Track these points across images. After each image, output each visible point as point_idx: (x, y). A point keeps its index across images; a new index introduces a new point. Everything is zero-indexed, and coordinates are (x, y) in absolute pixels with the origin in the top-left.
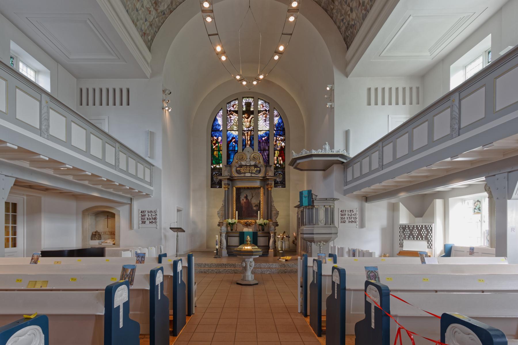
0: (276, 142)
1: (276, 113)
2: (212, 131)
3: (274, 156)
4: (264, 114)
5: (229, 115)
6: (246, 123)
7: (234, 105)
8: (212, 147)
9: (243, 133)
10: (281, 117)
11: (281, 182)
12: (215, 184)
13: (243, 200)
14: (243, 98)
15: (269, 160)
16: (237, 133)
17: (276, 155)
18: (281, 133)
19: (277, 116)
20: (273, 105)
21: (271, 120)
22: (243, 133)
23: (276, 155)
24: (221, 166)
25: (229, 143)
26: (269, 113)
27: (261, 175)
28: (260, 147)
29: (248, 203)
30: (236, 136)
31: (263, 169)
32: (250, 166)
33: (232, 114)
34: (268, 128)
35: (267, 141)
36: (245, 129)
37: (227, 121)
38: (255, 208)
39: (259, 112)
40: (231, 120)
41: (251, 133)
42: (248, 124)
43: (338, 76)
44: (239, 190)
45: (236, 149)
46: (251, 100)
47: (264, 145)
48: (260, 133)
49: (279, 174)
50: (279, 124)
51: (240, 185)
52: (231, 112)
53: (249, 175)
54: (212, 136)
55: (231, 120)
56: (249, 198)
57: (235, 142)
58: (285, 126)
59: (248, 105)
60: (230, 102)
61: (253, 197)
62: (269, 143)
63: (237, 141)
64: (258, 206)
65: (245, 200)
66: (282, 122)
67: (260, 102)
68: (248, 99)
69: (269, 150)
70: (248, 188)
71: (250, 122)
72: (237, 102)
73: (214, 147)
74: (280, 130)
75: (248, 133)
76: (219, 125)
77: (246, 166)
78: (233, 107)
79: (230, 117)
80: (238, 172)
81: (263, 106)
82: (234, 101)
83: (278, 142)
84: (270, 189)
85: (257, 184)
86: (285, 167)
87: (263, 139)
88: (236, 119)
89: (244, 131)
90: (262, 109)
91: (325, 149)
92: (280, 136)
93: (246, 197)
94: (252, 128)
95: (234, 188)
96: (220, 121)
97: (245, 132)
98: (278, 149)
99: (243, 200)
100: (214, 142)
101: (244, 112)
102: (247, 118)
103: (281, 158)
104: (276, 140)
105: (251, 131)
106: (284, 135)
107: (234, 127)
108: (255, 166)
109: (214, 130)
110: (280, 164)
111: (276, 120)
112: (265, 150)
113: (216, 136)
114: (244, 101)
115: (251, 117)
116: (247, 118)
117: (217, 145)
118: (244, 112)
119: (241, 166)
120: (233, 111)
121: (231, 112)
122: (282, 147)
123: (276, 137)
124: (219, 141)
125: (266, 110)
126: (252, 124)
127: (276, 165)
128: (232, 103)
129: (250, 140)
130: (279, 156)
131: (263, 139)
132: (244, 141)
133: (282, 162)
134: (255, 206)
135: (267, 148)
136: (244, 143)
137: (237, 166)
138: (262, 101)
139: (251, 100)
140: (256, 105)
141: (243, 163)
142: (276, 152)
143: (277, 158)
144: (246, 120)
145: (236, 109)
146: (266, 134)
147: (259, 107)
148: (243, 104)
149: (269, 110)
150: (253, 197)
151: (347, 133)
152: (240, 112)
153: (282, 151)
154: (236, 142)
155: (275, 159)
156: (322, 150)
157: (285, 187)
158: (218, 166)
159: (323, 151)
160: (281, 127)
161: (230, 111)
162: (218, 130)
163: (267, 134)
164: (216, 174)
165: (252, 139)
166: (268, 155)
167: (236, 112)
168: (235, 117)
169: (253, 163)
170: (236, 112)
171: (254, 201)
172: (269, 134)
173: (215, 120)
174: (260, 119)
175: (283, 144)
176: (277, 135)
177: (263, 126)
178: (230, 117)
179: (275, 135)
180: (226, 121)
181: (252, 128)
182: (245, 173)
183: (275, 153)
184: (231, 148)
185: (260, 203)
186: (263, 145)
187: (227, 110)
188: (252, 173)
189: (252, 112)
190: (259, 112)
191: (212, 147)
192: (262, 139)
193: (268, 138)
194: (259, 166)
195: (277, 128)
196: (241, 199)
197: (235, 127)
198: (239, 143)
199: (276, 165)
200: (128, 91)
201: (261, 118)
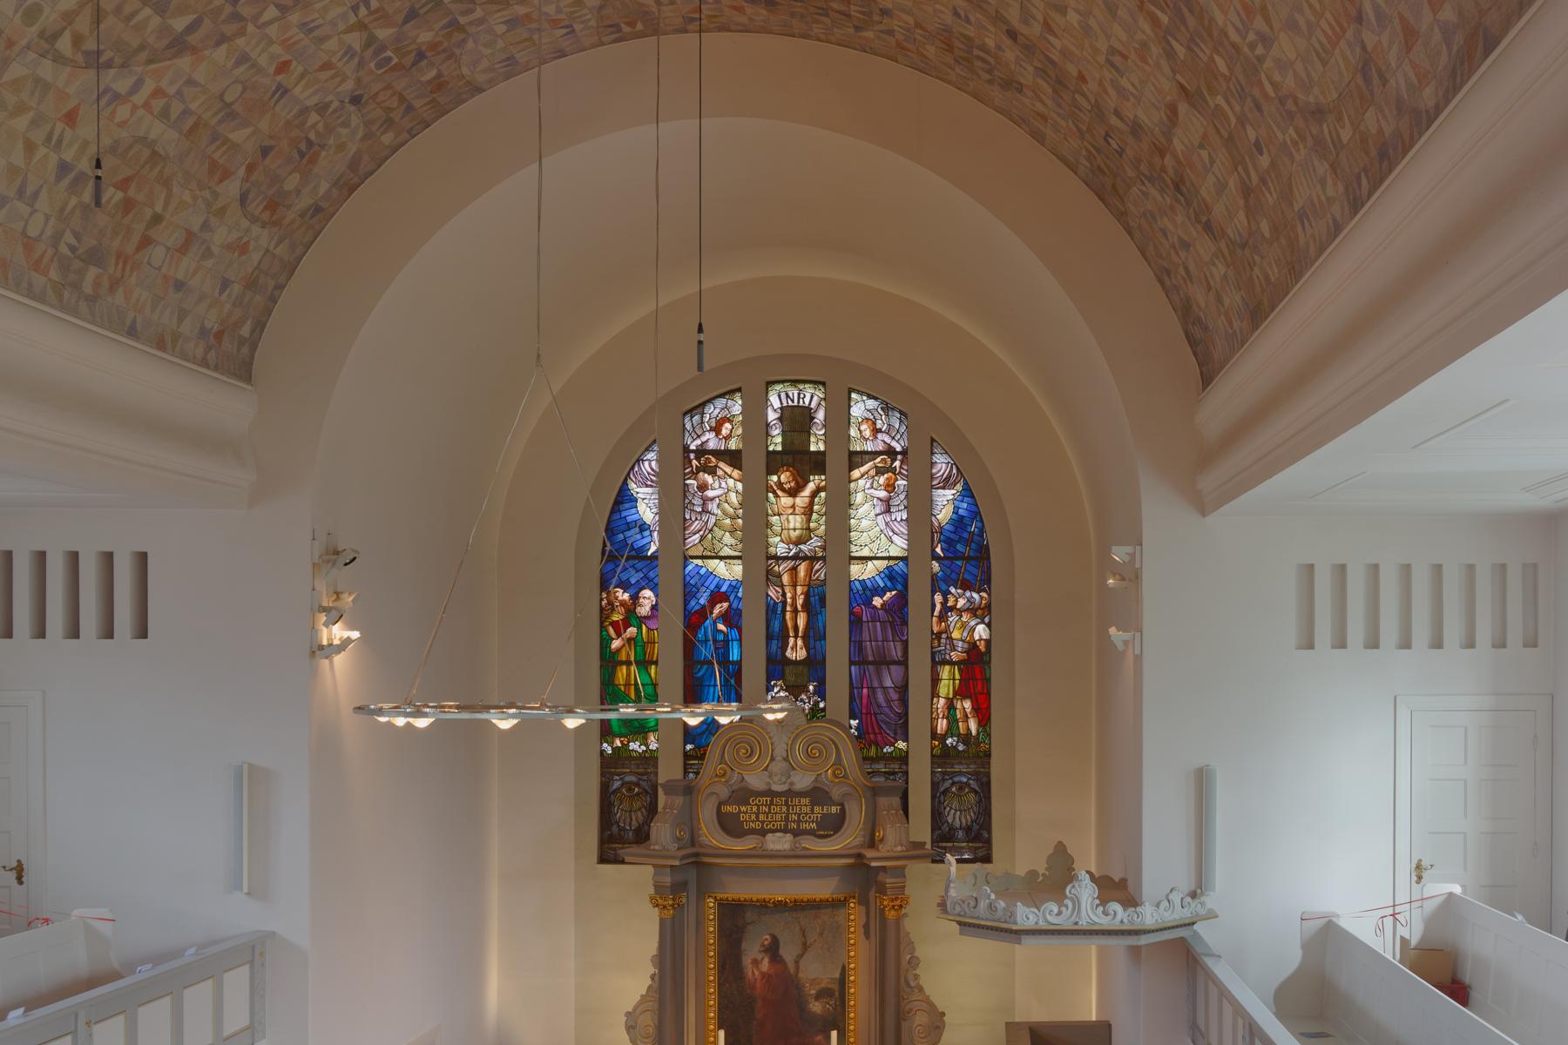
0: (943, 617)
1: (941, 464)
2: (611, 558)
3: (935, 694)
4: (880, 471)
5: (694, 475)
6: (788, 518)
7: (721, 423)
8: (605, 642)
9: (769, 572)
10: (966, 483)
11: (968, 829)
12: (616, 841)
13: (756, 962)
14: (770, 383)
15: (905, 715)
16: (737, 570)
17: (946, 688)
18: (969, 571)
19: (947, 483)
20: (927, 430)
21: (919, 506)
22: (769, 572)
23: (946, 688)
24: (653, 746)
25: (694, 620)
26: (907, 466)
27: (849, 839)
28: (857, 645)
29: (785, 986)
30: (734, 587)
31: (857, 816)
32: (790, 794)
33: (712, 472)
34: (898, 547)
35: (898, 609)
36: (781, 550)
37: (686, 506)
38: (816, 1007)
39: (855, 459)
40: (705, 500)
41: (810, 570)
42: (796, 521)
43: (1160, 512)
44: (734, 917)
45: (734, 655)
46: (811, 396)
47: (884, 615)
48: (856, 571)
49: (962, 786)
50: (959, 522)
51: (741, 890)
52: (707, 460)
53: (779, 842)
54: (604, 585)
55: (705, 500)
56: (788, 953)
57: (726, 618)
58: (991, 537)
59: (797, 420)
60: (703, 404)
61: (805, 947)
62: (905, 623)
63: (739, 613)
64: (838, 993)
65: (765, 965)
66: (976, 514)
67: (860, 408)
68: (793, 393)
69: (904, 663)
70: (780, 906)
71: (808, 511)
72: (737, 407)
73: (616, 644)
74: (965, 554)
75: (794, 569)
76: (643, 527)
77: (770, 793)
78: (717, 429)
79: (703, 487)
80: (730, 826)
81: (876, 431)
82: (721, 402)
83: (953, 618)
84: (891, 915)
85: (822, 889)
86: (988, 755)
87: (877, 602)
88: (733, 497)
89: (777, 558)
90: (869, 447)
91: (1077, 902)
92: (966, 586)
93: (773, 950)
94: (815, 542)
95: (711, 902)
96: (646, 509)
97: (783, 567)
98: (955, 656)
99: (754, 962)
100: (616, 617)
101: (774, 462)
102: (793, 493)
103: (968, 704)
104: (947, 609)
105: (812, 559)
106: (983, 582)
107: (720, 533)
108: (817, 795)
109: (620, 555)
110: (966, 738)
111: (945, 504)
112: (883, 661)
113: (625, 586)
114: (774, 400)
115: (811, 486)
116: (793, 493)
117: (632, 631)
118: (774, 462)
119: (743, 795)
120: (717, 453)
121: (707, 460)
122: (972, 647)
123: (945, 594)
124: (644, 610)
125: (891, 452)
126: (819, 525)
127: (943, 738)
128: (713, 411)
129: (806, 605)
130: (961, 693)
131: (877, 602)
132: (773, 611)
133: (973, 725)
134: (818, 997)
135: (895, 651)
136: (776, 625)
137: (724, 792)
138: (871, 404)
139: (811, 396)
140: (840, 419)
141: (756, 781)
142: (945, 672)
143: (950, 706)
144: (786, 501)
145: (733, 445)
146: (890, 574)
147: (853, 432)
148: (772, 416)
149: (904, 453)
150: (805, 947)
151: (1202, 783)
152: (757, 462)
153: (976, 665)
154: (732, 618)
155: (938, 704)
156: (1060, 903)
157: (987, 859)
158: (634, 746)
159: (1066, 913)
160: (967, 542)
161: (701, 452)
162: (639, 554)
163: (895, 577)
164: (629, 786)
165: (815, 602)
166: (903, 689)
167: (733, 458)
168: (726, 488)
169: (802, 781)
170: (733, 458)
171: (815, 972)
172: (905, 577)
173: (624, 498)
174: (859, 498)
175: (981, 631)
176: (949, 581)
177: (877, 535)
178: (703, 487)
179: (936, 584)
180: (676, 505)
181: (815, 542)
182: (763, 833)
183: (936, 680)
184: (706, 652)
185: (842, 981)
186: (873, 632)
187: (686, 450)
188: (797, 833)
189: (818, 463)
190: (855, 459)
191: (605, 642)
192: (868, 602)
193: (901, 603)
194: (836, 793)
195: (949, 543)
196: (747, 961)
197: (728, 539)
198: (746, 623)
199: (943, 738)
200: (142, 558)
201: (866, 491)
